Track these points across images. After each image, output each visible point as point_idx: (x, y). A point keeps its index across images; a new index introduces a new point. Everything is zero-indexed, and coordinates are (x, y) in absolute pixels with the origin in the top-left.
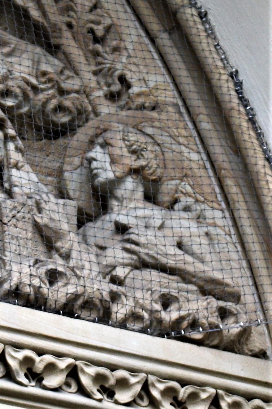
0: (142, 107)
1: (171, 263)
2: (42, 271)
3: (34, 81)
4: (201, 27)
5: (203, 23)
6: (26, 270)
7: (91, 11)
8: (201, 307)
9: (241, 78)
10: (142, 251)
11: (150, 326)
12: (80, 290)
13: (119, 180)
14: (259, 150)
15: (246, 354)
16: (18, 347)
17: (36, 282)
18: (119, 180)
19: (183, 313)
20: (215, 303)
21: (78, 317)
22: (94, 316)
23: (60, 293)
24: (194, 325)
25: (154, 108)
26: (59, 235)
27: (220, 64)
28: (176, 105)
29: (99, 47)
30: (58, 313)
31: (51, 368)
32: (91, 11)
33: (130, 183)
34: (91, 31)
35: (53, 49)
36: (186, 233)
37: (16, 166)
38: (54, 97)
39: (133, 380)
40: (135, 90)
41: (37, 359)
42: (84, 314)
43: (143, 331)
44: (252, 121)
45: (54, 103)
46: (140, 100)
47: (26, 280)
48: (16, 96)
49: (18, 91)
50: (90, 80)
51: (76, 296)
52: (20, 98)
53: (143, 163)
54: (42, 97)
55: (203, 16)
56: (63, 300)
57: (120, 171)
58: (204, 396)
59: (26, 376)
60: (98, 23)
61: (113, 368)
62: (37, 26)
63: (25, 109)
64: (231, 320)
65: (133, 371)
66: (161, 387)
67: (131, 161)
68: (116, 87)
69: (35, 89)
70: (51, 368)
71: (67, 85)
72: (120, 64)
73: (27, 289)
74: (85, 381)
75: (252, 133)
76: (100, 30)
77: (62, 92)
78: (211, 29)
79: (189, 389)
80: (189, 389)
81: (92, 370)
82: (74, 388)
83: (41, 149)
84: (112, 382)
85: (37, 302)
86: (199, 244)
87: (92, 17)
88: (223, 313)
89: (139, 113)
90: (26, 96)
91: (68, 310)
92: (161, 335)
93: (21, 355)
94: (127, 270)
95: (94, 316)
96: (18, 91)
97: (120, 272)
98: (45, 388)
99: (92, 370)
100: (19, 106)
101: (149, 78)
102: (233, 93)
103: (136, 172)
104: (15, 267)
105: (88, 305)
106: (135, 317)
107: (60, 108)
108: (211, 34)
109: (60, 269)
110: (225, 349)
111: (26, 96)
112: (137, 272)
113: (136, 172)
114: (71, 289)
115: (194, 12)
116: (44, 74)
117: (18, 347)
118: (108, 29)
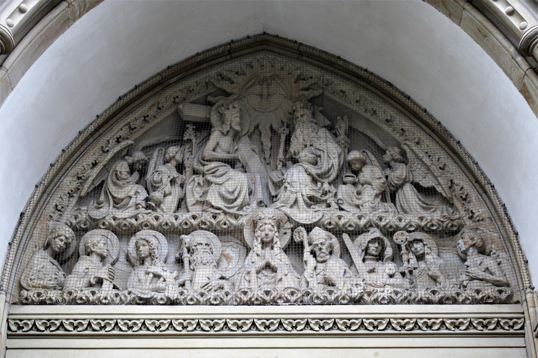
0: (479, 221)
1: (481, 277)
2: (429, 291)
3: (442, 219)
4: (491, 191)
5: (492, 189)
6: (423, 292)
7: (460, 190)
8: (490, 291)
9: (506, 206)
10: (471, 275)
11: (472, 301)
12: (443, 295)
13: (467, 250)
14: (511, 231)
15: (512, 304)
16: (421, 319)
17: (427, 296)
18: (467, 250)
19: (483, 295)
20: (497, 288)
21: (445, 304)
22: (451, 302)
23: (437, 297)
24: (489, 297)
25: (483, 220)
26: (438, 277)
27: (498, 203)
28: (490, 218)
29: (464, 202)
30: (437, 304)
31: (434, 323)
32: (460, 190)
33: (471, 250)
34: (461, 197)
35: (452, 205)
36: (489, 265)
37: (428, 254)
38: (449, 223)
39: (465, 322)
40: (477, 214)
41: (429, 321)
42: (447, 302)
43: (470, 304)
44: (509, 221)
45: (450, 225)
46: (478, 219)
47: (423, 296)
48: (436, 226)
49: (436, 224)
50: (463, 213)
51: (442, 298)
52: (437, 226)
53: (474, 242)
54: (445, 224)
55: (493, 187)
56: (438, 300)
57: (467, 246)
58: (493, 322)
59: (426, 327)
60: (464, 194)
61: (457, 319)
62: (445, 198)
63: (441, 229)
64: (503, 293)
65: (465, 319)
66: (476, 322)
67: (471, 243)
68: (471, 214)
69: (443, 222)
70: (434, 323)
71: (453, 217)
72: (471, 207)
73: (424, 299)
74: (447, 325)
75: (509, 226)
76: (464, 196)
77: (452, 220)
78: (496, 191)
79: (487, 321)
80: (487, 321)
81: (449, 321)
82: (445, 328)
83: (450, 240)
84: (457, 324)
85: (429, 302)
86: (494, 267)
87: (461, 192)
88: (500, 292)
89: (477, 224)
90: (439, 225)
91: (441, 302)
92: (477, 304)
93: (422, 321)
94: (468, 281)
95: (451, 302)
96: (436, 224)
97: (465, 283)
98: (433, 330)
99: (449, 321)
100: (438, 228)
101: (480, 210)
102: (503, 212)
103: (473, 245)
104: (420, 292)
105: (448, 299)
106: (467, 299)
107: (452, 226)
108: (495, 193)
109: (436, 289)
110: (504, 303)
111: (439, 225)
112: (471, 282)
113: (473, 245)
114: (440, 296)
115: (489, 186)
116: (444, 216)
117: (421, 319)
118: (467, 195)
